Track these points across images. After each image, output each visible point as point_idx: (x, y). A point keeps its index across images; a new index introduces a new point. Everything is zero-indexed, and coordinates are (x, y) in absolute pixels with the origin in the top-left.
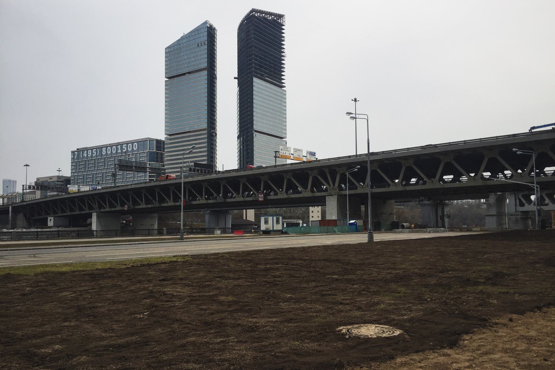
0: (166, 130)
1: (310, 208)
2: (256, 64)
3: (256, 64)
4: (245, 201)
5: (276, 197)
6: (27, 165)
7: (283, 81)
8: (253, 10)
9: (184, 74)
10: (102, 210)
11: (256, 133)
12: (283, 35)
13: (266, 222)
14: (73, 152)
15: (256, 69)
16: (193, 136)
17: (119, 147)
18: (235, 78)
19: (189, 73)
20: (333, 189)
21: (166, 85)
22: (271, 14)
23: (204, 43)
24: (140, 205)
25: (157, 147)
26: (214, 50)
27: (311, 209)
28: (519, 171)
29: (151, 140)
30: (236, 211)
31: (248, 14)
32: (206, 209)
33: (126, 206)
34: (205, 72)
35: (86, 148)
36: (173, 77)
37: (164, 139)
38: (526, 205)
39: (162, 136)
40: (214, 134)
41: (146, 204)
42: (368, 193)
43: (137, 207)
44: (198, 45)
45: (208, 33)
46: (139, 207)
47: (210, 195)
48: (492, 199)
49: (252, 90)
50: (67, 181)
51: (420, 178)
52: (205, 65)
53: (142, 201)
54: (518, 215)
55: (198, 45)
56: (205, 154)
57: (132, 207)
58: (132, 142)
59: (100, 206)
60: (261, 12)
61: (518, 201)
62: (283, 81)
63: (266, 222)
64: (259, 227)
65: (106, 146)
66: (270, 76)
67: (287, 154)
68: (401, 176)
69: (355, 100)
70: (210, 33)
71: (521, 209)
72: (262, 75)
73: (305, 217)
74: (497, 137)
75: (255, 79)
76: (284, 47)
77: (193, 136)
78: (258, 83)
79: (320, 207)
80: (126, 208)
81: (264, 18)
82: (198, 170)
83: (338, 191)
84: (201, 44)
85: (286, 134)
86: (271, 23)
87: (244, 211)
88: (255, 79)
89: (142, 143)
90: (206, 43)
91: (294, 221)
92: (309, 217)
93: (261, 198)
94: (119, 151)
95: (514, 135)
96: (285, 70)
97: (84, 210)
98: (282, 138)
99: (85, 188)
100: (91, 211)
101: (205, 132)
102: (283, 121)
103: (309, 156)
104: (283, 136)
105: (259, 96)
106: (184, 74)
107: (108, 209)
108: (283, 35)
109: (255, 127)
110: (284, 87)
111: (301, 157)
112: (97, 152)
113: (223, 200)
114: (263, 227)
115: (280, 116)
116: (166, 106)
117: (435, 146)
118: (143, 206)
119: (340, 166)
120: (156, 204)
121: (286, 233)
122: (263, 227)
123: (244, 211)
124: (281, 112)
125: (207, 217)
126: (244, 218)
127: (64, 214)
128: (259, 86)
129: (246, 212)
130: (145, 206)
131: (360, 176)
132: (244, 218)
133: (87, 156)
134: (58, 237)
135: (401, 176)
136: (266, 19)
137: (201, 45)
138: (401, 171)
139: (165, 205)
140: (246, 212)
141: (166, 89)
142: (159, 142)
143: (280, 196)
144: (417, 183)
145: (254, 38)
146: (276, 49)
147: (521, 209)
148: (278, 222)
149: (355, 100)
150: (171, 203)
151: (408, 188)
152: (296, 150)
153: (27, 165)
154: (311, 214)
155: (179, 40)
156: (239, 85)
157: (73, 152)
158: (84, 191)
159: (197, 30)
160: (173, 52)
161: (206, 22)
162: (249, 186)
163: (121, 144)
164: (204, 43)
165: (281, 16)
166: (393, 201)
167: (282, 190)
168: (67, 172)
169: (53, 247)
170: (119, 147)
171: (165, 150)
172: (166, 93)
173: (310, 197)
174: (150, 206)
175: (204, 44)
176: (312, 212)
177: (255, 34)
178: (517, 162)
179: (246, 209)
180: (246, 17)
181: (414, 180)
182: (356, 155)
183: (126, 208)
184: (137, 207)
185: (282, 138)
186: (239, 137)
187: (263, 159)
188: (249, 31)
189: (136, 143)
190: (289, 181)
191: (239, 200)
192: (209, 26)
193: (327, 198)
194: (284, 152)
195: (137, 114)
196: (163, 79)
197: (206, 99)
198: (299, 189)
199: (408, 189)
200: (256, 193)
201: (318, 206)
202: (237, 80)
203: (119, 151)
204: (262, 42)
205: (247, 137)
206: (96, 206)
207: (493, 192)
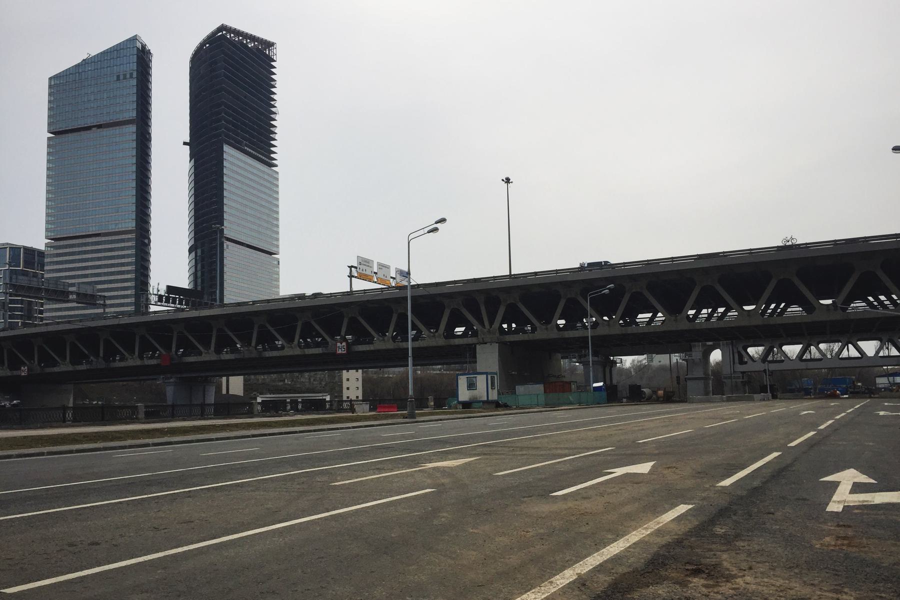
0: (47, 230)
1: (345, 372)
2: (227, 121)
3: (227, 121)
4: (305, 356)
5: (122, 364)
7: (272, 155)
8: (223, 28)
11: (228, 243)
12: (273, 77)
13: (471, 386)
18: (185, 143)
19: (99, 126)
20: (489, 331)
21: (49, 146)
22: (253, 38)
23: (131, 75)
25: (25, 262)
27: (345, 374)
28: (606, 318)
29: (15, 250)
32: (169, 376)
34: (133, 128)
36: (61, 131)
37: (42, 247)
39: (38, 241)
40: (146, 241)
41: (73, 363)
44: (118, 77)
46: (56, 369)
47: (362, 336)
51: (469, 327)
52: (133, 114)
54: (738, 378)
55: (118, 77)
56: (132, 276)
60: (238, 33)
61: (736, 356)
62: (272, 155)
63: (471, 386)
64: (455, 394)
67: (368, 272)
68: (237, 341)
69: (508, 181)
70: (135, 61)
71: (740, 368)
72: (239, 142)
73: (336, 388)
74: (672, 258)
75: (226, 148)
79: (360, 371)
80: (24, 371)
81: (241, 42)
82: (175, 299)
83: (497, 335)
84: (125, 75)
85: (278, 246)
87: (224, 379)
88: (226, 148)
90: (135, 75)
93: (341, 348)
95: (557, 271)
98: (271, 254)
101: (133, 236)
102: (272, 224)
103: (399, 278)
104: (273, 250)
105: (233, 178)
108: (273, 77)
109: (227, 233)
110: (276, 166)
111: (388, 278)
114: (464, 394)
115: (268, 215)
116: (48, 184)
119: (451, 296)
120: (102, 365)
121: (506, 406)
122: (464, 394)
124: (271, 210)
126: (224, 392)
129: (228, 381)
130: (70, 368)
132: (224, 392)
134: (64, 421)
135: (237, 341)
136: (246, 46)
137: (125, 78)
138: (360, 323)
139: (56, 369)
140: (228, 381)
142: (30, 252)
144: (465, 334)
146: (262, 101)
147: (740, 368)
149: (508, 181)
152: (381, 266)
154: (345, 384)
156: (192, 156)
160: (66, 88)
161: (134, 39)
162: (114, 342)
164: (131, 75)
165: (270, 45)
166: (560, 355)
169: (129, 442)
171: (46, 268)
172: (49, 161)
173: (441, 347)
174: (83, 367)
175: (131, 77)
176: (348, 380)
178: (605, 306)
179: (228, 376)
181: (460, 330)
182: (510, 276)
183: (24, 371)
185: (271, 254)
187: (239, 288)
192: (139, 45)
193: (478, 346)
194: (365, 267)
196: (44, 135)
197: (134, 177)
198: (279, 343)
199: (567, 336)
200: (329, 339)
201: (357, 369)
204: (235, 85)
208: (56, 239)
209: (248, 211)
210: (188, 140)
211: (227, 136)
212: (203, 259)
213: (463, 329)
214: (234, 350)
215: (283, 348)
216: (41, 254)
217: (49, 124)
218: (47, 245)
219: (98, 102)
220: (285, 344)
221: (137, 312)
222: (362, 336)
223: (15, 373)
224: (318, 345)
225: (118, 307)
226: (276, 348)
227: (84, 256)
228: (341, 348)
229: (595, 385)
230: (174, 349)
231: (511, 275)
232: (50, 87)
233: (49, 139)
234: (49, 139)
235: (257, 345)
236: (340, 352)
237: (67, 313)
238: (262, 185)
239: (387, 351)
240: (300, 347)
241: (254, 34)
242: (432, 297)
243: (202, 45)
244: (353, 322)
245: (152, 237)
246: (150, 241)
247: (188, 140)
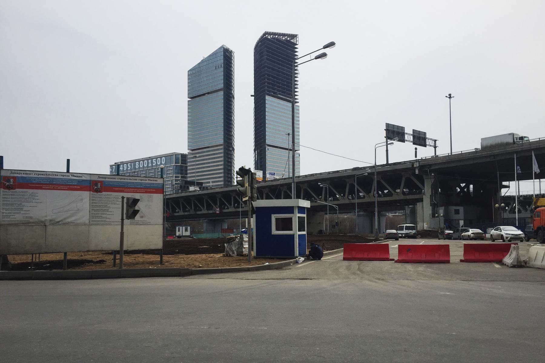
0: (189, 146)
2: (268, 83)
8: (266, 33)
9: (204, 95)
12: (296, 54)
14: (111, 166)
15: (268, 87)
16: (212, 151)
17: (150, 161)
18: (252, 96)
19: (208, 93)
21: (189, 105)
22: (284, 35)
24: (201, 210)
25: (182, 160)
26: (231, 71)
29: (176, 155)
30: (390, 215)
31: (262, 37)
34: (222, 93)
35: (123, 162)
36: (194, 97)
38: (523, 211)
39: (184, 150)
40: (231, 149)
41: (208, 209)
42: (375, 202)
43: (199, 213)
45: (224, 57)
48: (408, 210)
49: (265, 107)
52: (222, 86)
53: (204, 207)
58: (161, 157)
63: (179, 231)
65: (139, 161)
66: (283, 93)
68: (337, 193)
70: (226, 57)
75: (267, 97)
77: (212, 151)
78: (271, 101)
86: (284, 43)
88: (267, 97)
89: (168, 157)
93: (218, 211)
94: (150, 165)
96: (298, 86)
106: (204, 95)
108: (296, 54)
109: (268, 142)
112: (131, 165)
113: (194, 213)
117: (338, 172)
118: (181, 213)
120: (192, 212)
123: (247, 219)
125: (205, 225)
131: (395, 185)
133: (127, 169)
141: (189, 108)
142: (184, 156)
145: (267, 59)
148: (186, 230)
150: (232, 209)
155: (199, 64)
157: (111, 166)
159: (214, 55)
160: (195, 75)
162: (310, 192)
163: (151, 158)
165: (294, 36)
167: (344, 195)
170: (150, 161)
177: (267, 55)
180: (260, 39)
184: (199, 213)
186: (255, 150)
188: (262, 53)
189: (164, 158)
190: (235, 198)
191: (369, 201)
195: (163, 132)
196: (186, 99)
202: (253, 97)
203: (150, 165)
204: (277, 61)
205: (261, 151)
207: (407, 205)
209: (280, 129)
210: (253, 94)
211: (269, 91)
213: (464, 184)
214: (336, 199)
215: (364, 197)
217: (189, 94)
219: (211, 80)
220: (365, 195)
221: (226, 185)
224: (386, 195)
225: (214, 182)
226: (176, 212)
227: (214, 156)
229: (389, 231)
231: (387, 164)
232: (188, 75)
233: (189, 101)
234: (189, 101)
237: (217, 184)
241: (284, 32)
242: (339, 178)
244: (408, 180)
247: (253, 94)
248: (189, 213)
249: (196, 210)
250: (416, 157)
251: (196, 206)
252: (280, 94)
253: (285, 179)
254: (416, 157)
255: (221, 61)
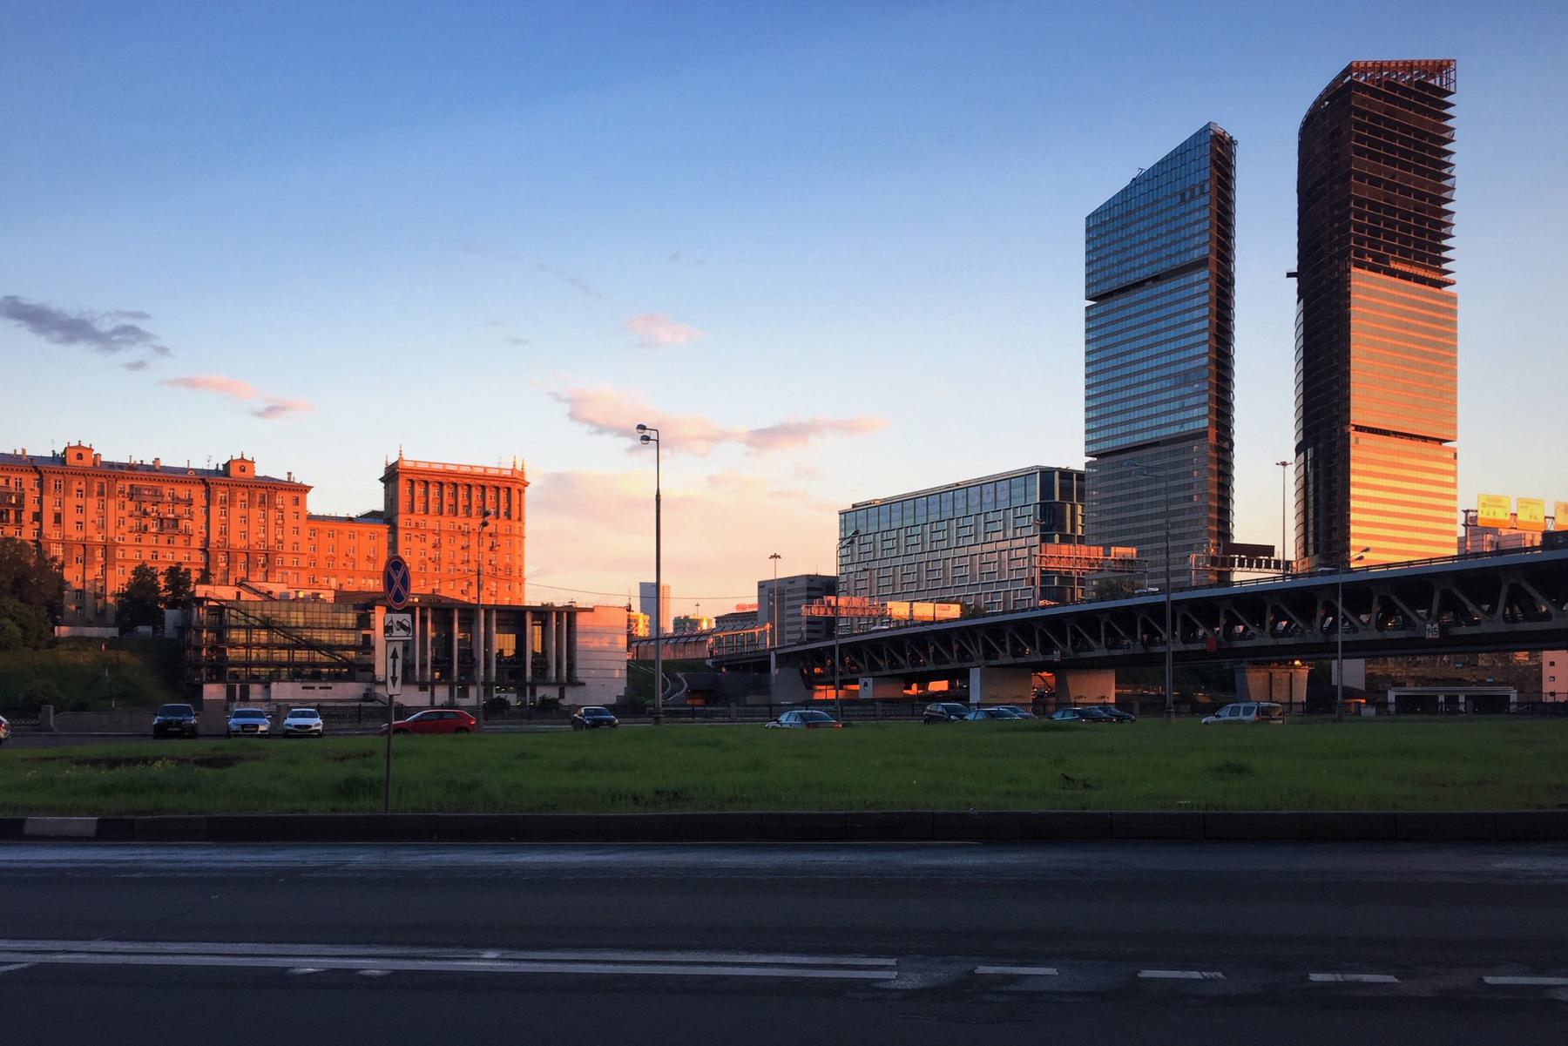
6: (775, 556)
7: (1445, 266)
9: (1139, 284)
10: (993, 662)
18: (1290, 275)
19: (1156, 279)
21: (1088, 320)
24: (1090, 649)
29: (1047, 474)
33: (1057, 653)
37: (1082, 468)
39: (1076, 460)
40: (1226, 445)
43: (1083, 655)
44: (1183, 195)
50: (820, 587)
53: (1098, 639)
55: (1183, 195)
57: (1072, 656)
59: (990, 653)
62: (1445, 266)
70: (1213, 157)
76: (1452, 159)
85: (1454, 427)
88: (1353, 270)
89: (1026, 475)
90: (1207, 188)
91: (1499, 690)
92: (1539, 679)
93: (1432, 631)
97: (947, 662)
98: (1441, 441)
99: (924, 610)
100: (966, 665)
106: (1139, 284)
107: (1009, 660)
113: (1142, 651)
127: (896, 672)
128: (1372, 296)
129: (1340, 668)
137: (1192, 190)
142: (1066, 474)
143: (1488, 627)
151: (1192, 647)
153: (775, 556)
156: (1302, 293)
158: (948, 620)
161: (1207, 128)
168: (829, 568)
174: (1119, 652)
183: (1056, 656)
184: (1083, 655)
185: (1441, 441)
194: (1491, 510)
206: (977, 651)
208: (1099, 456)
212: (1315, 464)
216: (1081, 476)
218: (1088, 465)
222: (1047, 647)
223: (1049, 658)
226: (919, 665)
228: (1432, 631)
230: (1318, 620)
234: (1088, 309)
235: (1440, 613)
236: (1429, 636)
238: (1108, 392)
239: (1497, 634)
240: (1506, 620)
243: (1318, 103)
245: (1235, 439)
246: (1232, 444)
248: (1126, 652)
249: (1015, 654)
250: (1359, 428)
251: (962, 651)
252: (1396, 260)
253: (1478, 555)
254: (1359, 428)
255: (1203, 172)
